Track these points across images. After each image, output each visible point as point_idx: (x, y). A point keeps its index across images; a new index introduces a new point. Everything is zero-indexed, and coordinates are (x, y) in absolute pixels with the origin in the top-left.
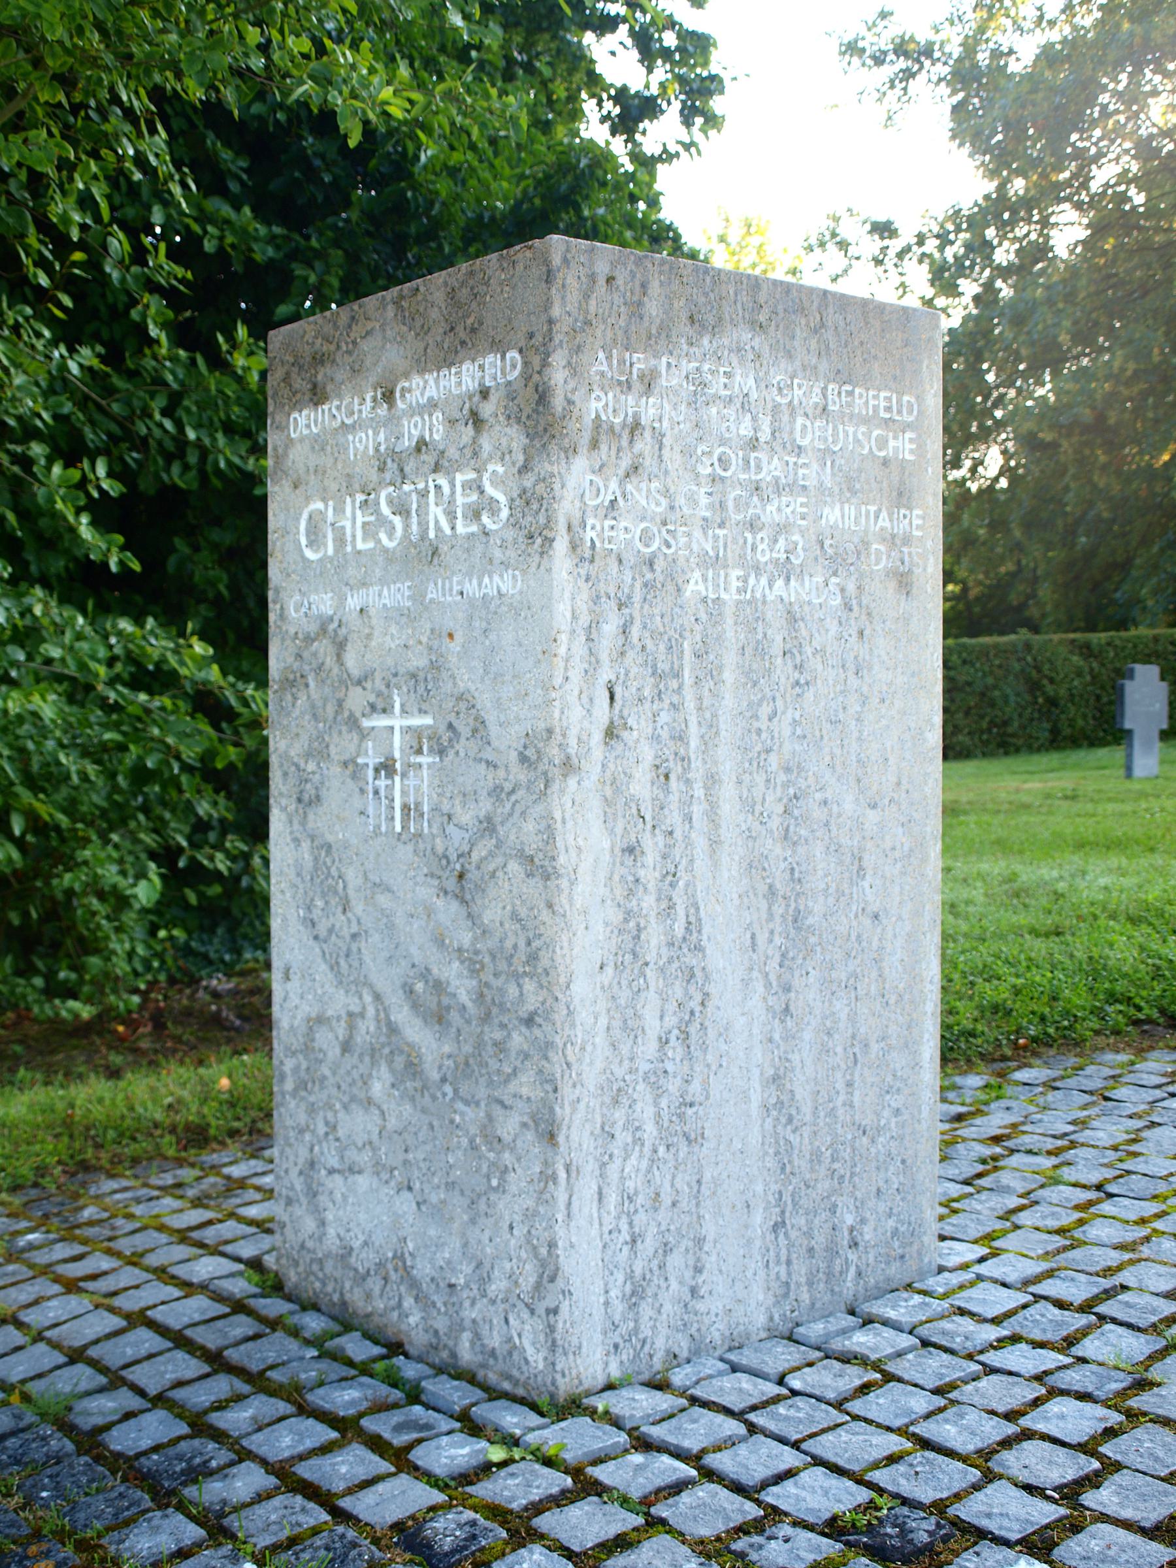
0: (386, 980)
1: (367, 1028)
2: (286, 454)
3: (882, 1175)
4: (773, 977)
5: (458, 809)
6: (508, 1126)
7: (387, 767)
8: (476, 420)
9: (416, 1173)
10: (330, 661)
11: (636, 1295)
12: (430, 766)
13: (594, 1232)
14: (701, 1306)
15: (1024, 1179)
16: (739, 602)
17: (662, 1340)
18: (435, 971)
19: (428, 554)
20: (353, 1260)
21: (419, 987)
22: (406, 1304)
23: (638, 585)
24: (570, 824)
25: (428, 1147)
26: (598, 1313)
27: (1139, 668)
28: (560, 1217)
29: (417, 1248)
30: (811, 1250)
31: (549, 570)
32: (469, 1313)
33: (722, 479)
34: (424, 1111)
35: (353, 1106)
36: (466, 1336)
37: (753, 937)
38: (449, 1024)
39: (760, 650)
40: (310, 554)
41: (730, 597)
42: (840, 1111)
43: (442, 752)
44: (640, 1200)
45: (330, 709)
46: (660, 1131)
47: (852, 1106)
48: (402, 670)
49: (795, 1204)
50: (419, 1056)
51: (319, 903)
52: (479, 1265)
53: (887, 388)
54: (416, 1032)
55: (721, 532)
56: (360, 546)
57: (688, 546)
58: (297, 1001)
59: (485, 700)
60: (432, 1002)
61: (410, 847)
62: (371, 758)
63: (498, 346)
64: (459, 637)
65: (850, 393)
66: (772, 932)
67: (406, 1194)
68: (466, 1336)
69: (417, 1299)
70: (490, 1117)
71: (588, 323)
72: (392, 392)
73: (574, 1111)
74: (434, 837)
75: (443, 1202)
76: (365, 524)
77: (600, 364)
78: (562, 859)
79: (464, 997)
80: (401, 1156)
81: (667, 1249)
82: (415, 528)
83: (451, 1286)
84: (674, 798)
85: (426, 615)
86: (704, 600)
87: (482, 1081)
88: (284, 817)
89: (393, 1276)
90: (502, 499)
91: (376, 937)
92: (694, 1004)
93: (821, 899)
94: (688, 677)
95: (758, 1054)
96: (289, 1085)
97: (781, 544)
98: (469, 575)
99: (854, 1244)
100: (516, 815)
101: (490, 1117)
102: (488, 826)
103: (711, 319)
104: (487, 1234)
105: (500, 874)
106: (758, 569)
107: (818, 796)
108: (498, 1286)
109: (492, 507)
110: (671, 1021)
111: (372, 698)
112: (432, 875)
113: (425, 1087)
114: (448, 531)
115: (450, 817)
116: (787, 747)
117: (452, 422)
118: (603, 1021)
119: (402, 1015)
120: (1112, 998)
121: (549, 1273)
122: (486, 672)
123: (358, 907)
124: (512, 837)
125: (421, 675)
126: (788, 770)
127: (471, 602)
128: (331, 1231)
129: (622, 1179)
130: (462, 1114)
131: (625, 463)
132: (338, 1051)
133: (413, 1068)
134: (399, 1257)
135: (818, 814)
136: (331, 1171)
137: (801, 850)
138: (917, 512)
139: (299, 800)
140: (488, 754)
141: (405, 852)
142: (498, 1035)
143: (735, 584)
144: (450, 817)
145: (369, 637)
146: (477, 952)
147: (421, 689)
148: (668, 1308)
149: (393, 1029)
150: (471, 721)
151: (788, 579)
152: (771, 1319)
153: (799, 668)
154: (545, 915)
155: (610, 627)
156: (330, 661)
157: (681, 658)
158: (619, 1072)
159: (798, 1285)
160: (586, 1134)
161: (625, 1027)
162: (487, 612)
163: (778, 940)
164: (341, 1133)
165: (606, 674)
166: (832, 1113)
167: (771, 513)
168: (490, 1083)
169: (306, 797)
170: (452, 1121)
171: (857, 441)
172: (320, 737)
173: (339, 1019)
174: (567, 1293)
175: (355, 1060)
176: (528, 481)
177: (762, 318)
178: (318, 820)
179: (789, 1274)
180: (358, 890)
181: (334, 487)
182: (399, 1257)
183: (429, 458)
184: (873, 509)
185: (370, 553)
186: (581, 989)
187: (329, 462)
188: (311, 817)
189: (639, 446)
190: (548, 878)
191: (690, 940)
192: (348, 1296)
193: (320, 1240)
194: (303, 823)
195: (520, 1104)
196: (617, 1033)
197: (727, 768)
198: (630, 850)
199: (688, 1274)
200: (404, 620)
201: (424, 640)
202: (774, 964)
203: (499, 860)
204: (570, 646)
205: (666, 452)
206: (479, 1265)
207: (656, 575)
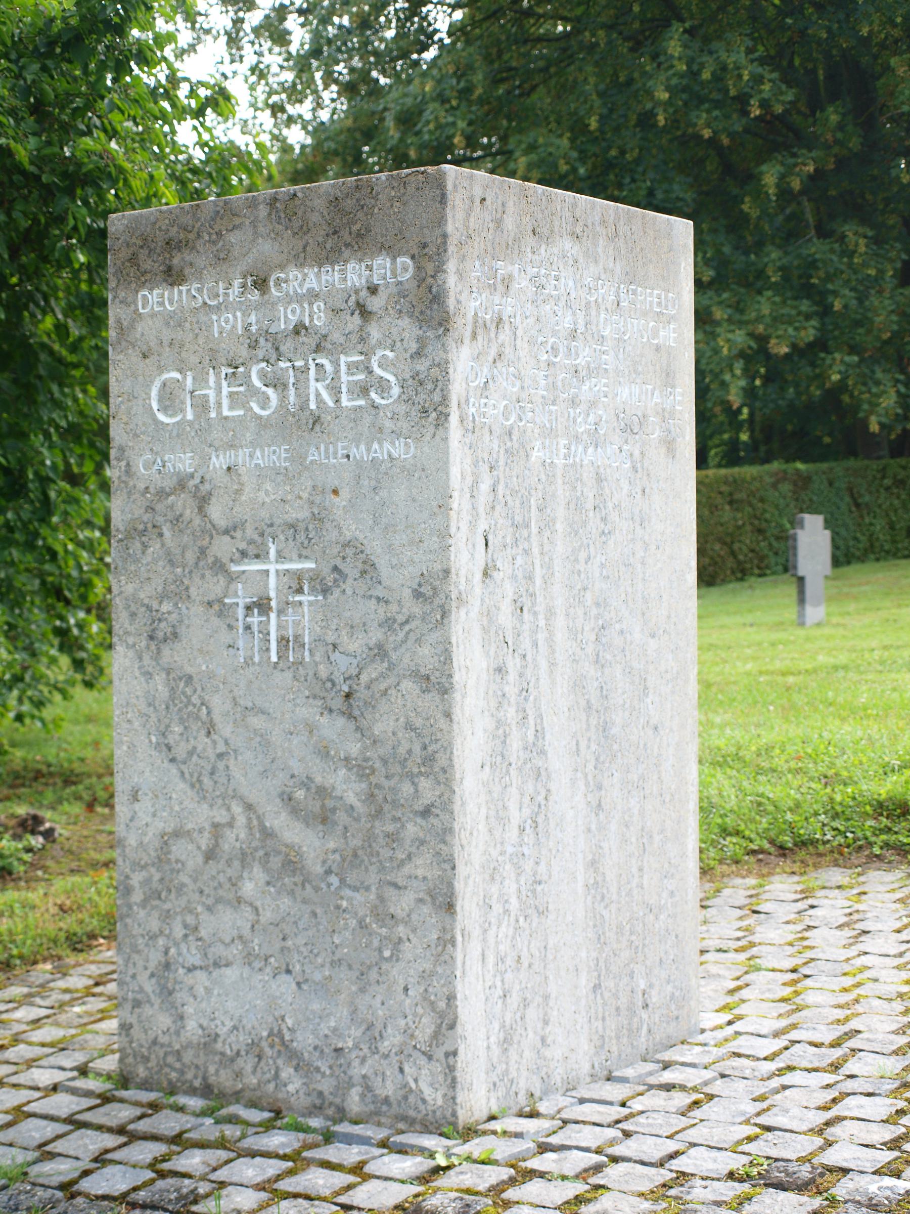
0: (263, 794)
2: (132, 326)
4: (590, 778)
6: (402, 903)
7: (262, 605)
8: (364, 312)
11: (506, 1042)
12: (311, 604)
14: (548, 1053)
15: (729, 969)
16: (566, 465)
17: (526, 1082)
18: (318, 779)
20: (219, 1046)
21: (300, 794)
22: (284, 1075)
23: (502, 451)
25: (310, 933)
27: (807, 518)
30: (618, 1009)
32: (357, 1071)
33: (554, 364)
34: (305, 901)
38: (335, 823)
40: (161, 417)
42: (635, 892)
43: (325, 591)
44: (509, 961)
45: (190, 556)
48: (278, 521)
49: (607, 969)
55: (553, 408)
56: (226, 413)
58: (149, 820)
59: (375, 547)
61: (289, 675)
62: (241, 597)
63: (393, 252)
64: (345, 493)
67: (284, 977)
69: (297, 1068)
70: (381, 899)
72: (265, 281)
73: (466, 884)
74: (316, 664)
75: (330, 977)
76: (231, 395)
77: (476, 271)
78: (457, 678)
79: (351, 798)
80: (278, 945)
81: (525, 1004)
82: (292, 399)
83: (337, 1050)
84: (526, 627)
88: (131, 653)
89: (268, 1052)
90: (392, 378)
91: (249, 755)
92: (540, 799)
94: (534, 529)
97: (591, 419)
99: (646, 1006)
100: (410, 643)
101: (381, 899)
102: (380, 652)
103: (545, 231)
104: (379, 999)
105: (392, 692)
107: (617, 626)
108: (392, 1040)
109: (383, 387)
110: (527, 812)
111: (243, 546)
112: (315, 697)
114: (331, 404)
115: (335, 646)
117: (336, 311)
118: (484, 811)
119: (279, 821)
120: (725, 832)
121: (447, 1022)
123: (225, 729)
124: (406, 660)
125: (302, 526)
126: (598, 605)
127: (359, 464)
131: (493, 352)
132: (200, 859)
133: (292, 864)
134: (276, 1035)
136: (191, 969)
137: (607, 671)
138: (679, 390)
139: (151, 638)
140: (379, 591)
141: (284, 678)
142: (390, 828)
144: (335, 646)
145: (239, 492)
146: (366, 760)
147: (301, 537)
148: (527, 1054)
149: (267, 834)
150: (360, 565)
153: (604, 520)
154: (442, 723)
155: (485, 487)
158: (495, 853)
162: (379, 474)
163: (594, 747)
164: (203, 933)
165: (483, 526)
166: (629, 893)
167: (586, 390)
168: (382, 869)
169: (160, 635)
170: (338, 907)
173: (201, 831)
176: (421, 366)
177: (578, 230)
178: (175, 655)
181: (194, 359)
182: (276, 1035)
183: (312, 341)
185: (240, 420)
189: (502, 337)
192: (212, 1080)
193: (178, 1033)
195: (415, 883)
198: (499, 670)
199: (540, 1025)
200: (280, 478)
201: (305, 495)
202: (590, 766)
203: (392, 680)
205: (519, 342)
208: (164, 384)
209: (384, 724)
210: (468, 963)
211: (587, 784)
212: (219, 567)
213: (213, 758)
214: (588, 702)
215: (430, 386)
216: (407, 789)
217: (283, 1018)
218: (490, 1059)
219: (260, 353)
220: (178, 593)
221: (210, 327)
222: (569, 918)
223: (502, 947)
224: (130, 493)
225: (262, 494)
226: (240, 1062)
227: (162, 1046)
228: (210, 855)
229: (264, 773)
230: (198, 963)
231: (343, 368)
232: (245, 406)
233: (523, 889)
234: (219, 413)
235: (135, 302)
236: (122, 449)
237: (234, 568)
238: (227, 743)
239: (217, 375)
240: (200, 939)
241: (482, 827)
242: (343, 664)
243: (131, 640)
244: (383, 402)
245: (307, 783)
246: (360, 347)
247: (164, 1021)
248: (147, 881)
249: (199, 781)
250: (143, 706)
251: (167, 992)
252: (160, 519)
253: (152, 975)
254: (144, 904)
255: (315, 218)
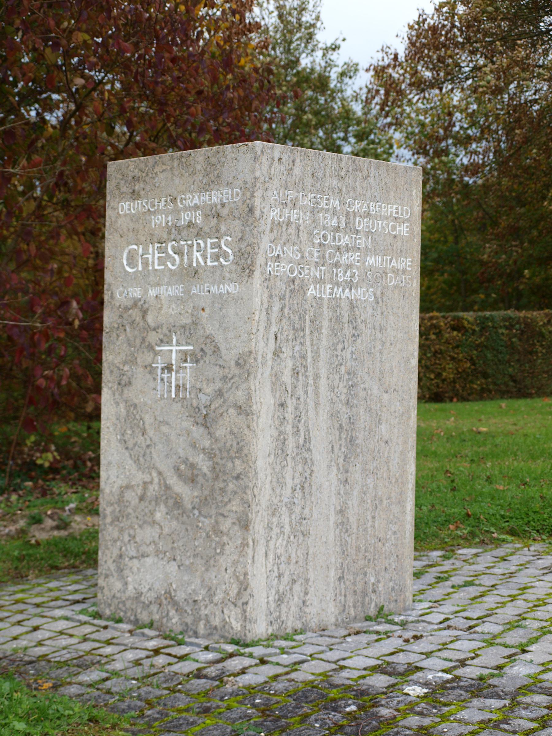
1: (153, 489)
2: (116, 222)
3: (387, 561)
4: (340, 466)
5: (205, 386)
6: (226, 525)
7: (168, 368)
9: (178, 552)
10: (138, 319)
11: (280, 600)
12: (190, 367)
13: (263, 570)
14: (307, 610)
16: (329, 299)
18: (191, 459)
19: (192, 273)
20: (142, 598)
21: (183, 467)
22: (171, 614)
24: (258, 392)
25: (185, 540)
26: (264, 606)
28: (250, 561)
29: (178, 587)
30: (355, 591)
31: (252, 284)
32: (204, 612)
33: (324, 245)
34: (183, 523)
35: (145, 525)
36: (202, 624)
37: (332, 447)
38: (197, 482)
39: (338, 320)
40: (128, 269)
41: (326, 296)
42: (369, 530)
43: (197, 361)
44: (283, 558)
45: (138, 342)
46: (291, 528)
47: (374, 527)
48: (177, 324)
49: (348, 570)
50: (181, 498)
51: (129, 432)
52: (210, 589)
53: (396, 203)
54: (180, 487)
55: (323, 268)
56: (156, 267)
57: (309, 274)
58: (115, 479)
59: (219, 338)
60: (189, 473)
61: (179, 404)
62: (159, 364)
64: (207, 310)
65: (380, 206)
66: (341, 445)
67: (173, 563)
68: (202, 624)
69: (177, 610)
70: (217, 522)
71: (271, 178)
73: (256, 516)
74: (192, 399)
75: (192, 564)
76: (159, 258)
78: (254, 407)
79: (205, 470)
80: (170, 546)
81: (294, 581)
82: (186, 261)
83: (195, 601)
84: (300, 383)
85: (190, 300)
86: (315, 298)
87: (214, 506)
88: (110, 392)
89: (164, 602)
90: (230, 251)
91: (160, 446)
93: (362, 433)
95: (333, 499)
96: (109, 520)
97: (348, 274)
98: (213, 284)
99: (374, 591)
100: (233, 389)
101: (217, 522)
102: (220, 393)
103: (320, 175)
105: (225, 414)
106: (338, 284)
107: (362, 386)
109: (226, 256)
110: (297, 481)
111: (161, 337)
112: (191, 416)
113: (184, 512)
114: (203, 264)
115: (200, 390)
116: (349, 363)
117: (206, 216)
118: (269, 478)
119: (172, 480)
122: (220, 326)
123: (151, 433)
126: (349, 374)
127: (214, 295)
128: (130, 587)
129: (275, 548)
130: (203, 522)
131: (284, 238)
132: (137, 501)
133: (178, 504)
135: (362, 394)
137: (354, 410)
139: (119, 384)
140: (221, 362)
141: (177, 407)
142: (222, 485)
143: (328, 291)
144: (200, 390)
145: (160, 309)
146: (212, 449)
148: (293, 608)
149: (168, 488)
151: (351, 289)
152: (337, 620)
153: (355, 328)
154: (246, 431)
155: (276, 309)
156: (138, 319)
157: (305, 323)
158: (276, 501)
159: (349, 606)
160: (261, 527)
161: (278, 481)
162: (222, 300)
163: (343, 449)
164: (137, 539)
165: (274, 329)
166: (365, 530)
167: (345, 259)
168: (217, 507)
169: (123, 382)
170: (197, 526)
171: (383, 227)
172: (132, 354)
173: (138, 485)
174: (251, 596)
175: (147, 504)
177: (343, 174)
178: (129, 393)
179: (345, 601)
180: (151, 425)
181: (143, 239)
183: (194, 231)
184: (389, 258)
185: (162, 271)
186: (260, 463)
187: (141, 227)
188: (126, 391)
189: (289, 231)
190: (248, 415)
191: (305, 446)
192: (139, 616)
193: (124, 592)
194: (122, 394)
195: (232, 514)
196: (275, 484)
197: (323, 372)
199: (302, 595)
200: (179, 302)
201: (190, 311)
202: (341, 460)
203: (225, 408)
204: (259, 316)
206: (210, 589)
207: (295, 286)
208: (129, 252)
209: (220, 432)
210: (256, 557)
211: (338, 469)
212: (151, 348)
213: (145, 447)
214: (341, 425)
215: (246, 256)
216: (230, 465)
217: (171, 584)
218: (268, 609)
219: (173, 237)
220: (132, 361)
221: (150, 222)
222: (324, 539)
223: (278, 551)
224: (112, 308)
225: (171, 310)
226: (152, 607)
227: (117, 598)
228: (142, 499)
229: (167, 456)
230: (135, 555)
231: (209, 245)
232: (164, 264)
233: (293, 521)
234: (153, 267)
235: (118, 208)
236: (109, 285)
237: (158, 348)
238: (151, 440)
239: (153, 247)
240: (136, 542)
241: (267, 486)
242: (204, 399)
243: (110, 385)
244: (226, 263)
245: (185, 461)
246: (216, 235)
247: (118, 585)
248: (113, 512)
249: (138, 459)
250: (114, 419)
251: (120, 570)
252: (125, 322)
253: (114, 561)
254: (111, 524)
255: (199, 167)
